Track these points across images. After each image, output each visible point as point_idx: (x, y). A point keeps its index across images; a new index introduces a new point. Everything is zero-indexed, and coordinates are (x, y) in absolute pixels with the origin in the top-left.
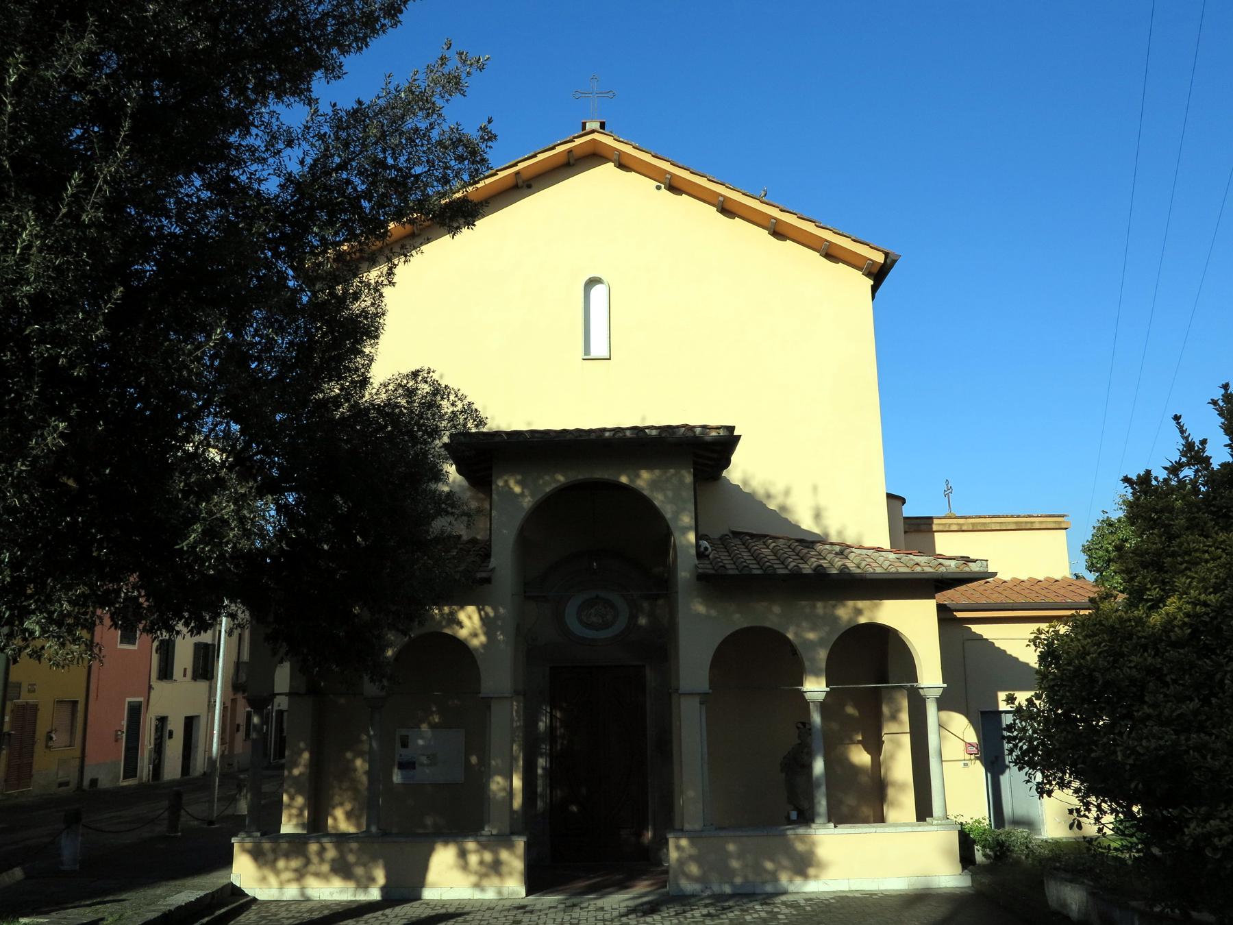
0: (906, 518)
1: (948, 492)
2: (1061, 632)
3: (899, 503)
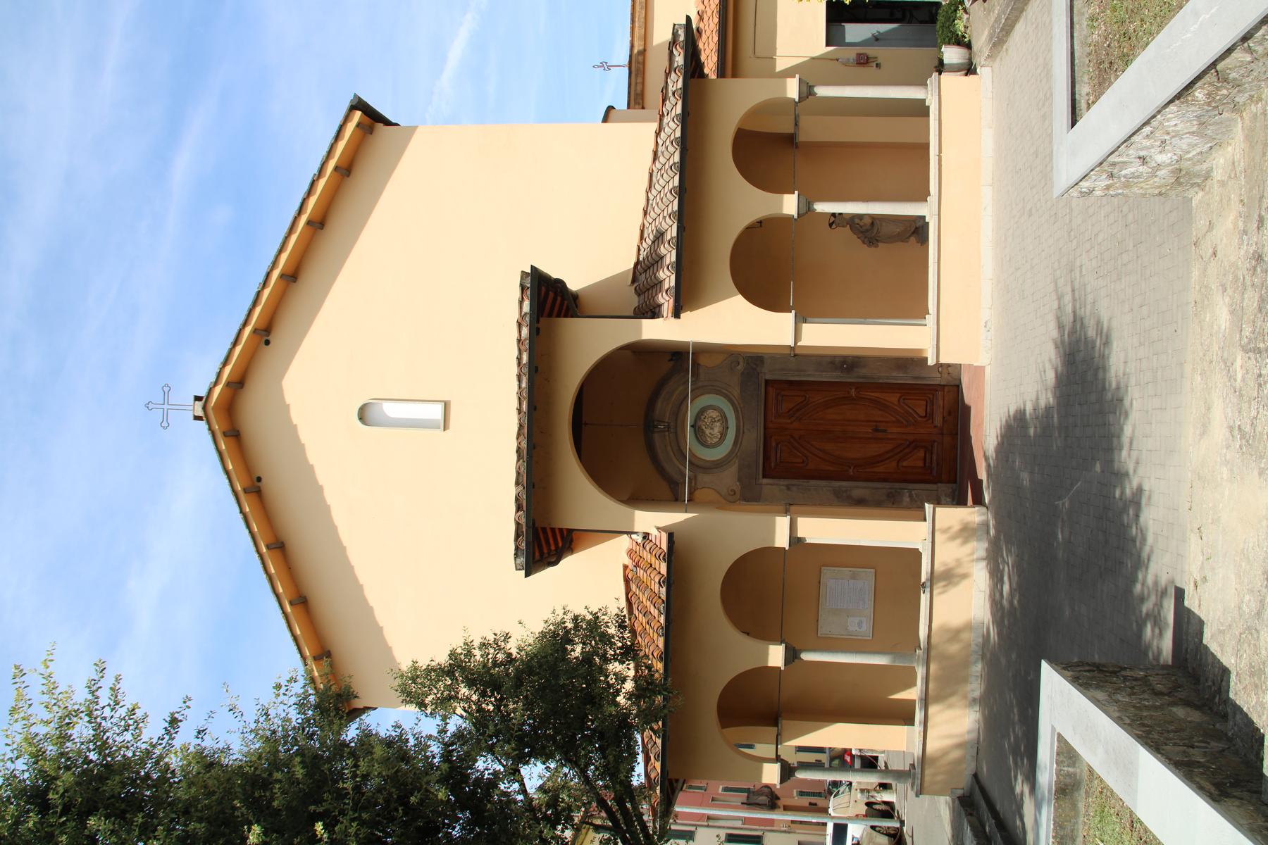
0: (629, 107)
1: (605, 66)
2: (618, 699)
3: (612, 112)
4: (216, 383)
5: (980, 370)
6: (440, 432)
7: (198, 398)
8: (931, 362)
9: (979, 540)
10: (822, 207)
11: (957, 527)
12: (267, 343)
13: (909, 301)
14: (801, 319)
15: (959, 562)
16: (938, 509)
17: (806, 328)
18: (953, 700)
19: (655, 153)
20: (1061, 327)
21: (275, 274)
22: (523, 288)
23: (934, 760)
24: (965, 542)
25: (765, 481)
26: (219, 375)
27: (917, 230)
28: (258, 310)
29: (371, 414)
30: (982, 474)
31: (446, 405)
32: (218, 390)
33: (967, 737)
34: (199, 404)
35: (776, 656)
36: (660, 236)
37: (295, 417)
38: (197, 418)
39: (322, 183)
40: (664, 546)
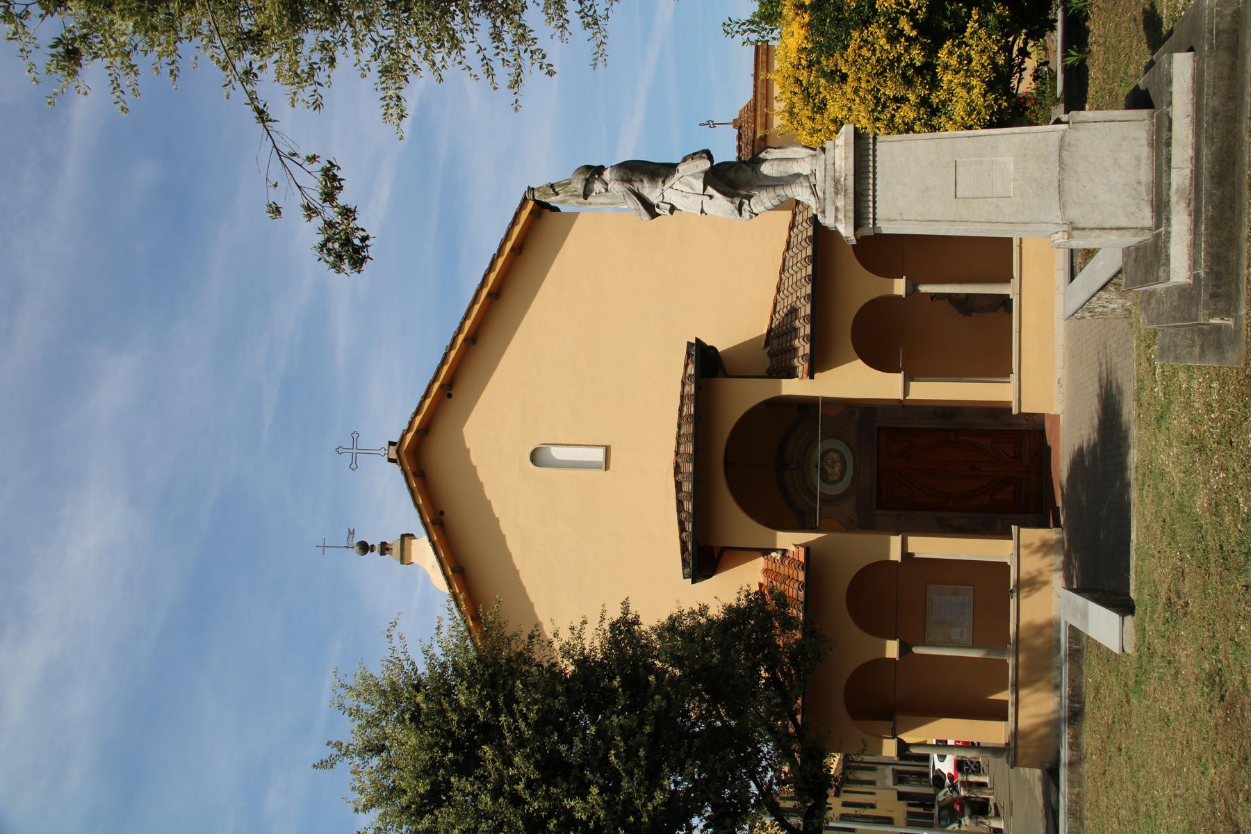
4: (408, 431)
5: (1056, 417)
6: (601, 472)
7: (391, 444)
8: (1015, 411)
9: (1056, 553)
10: (924, 289)
11: (1037, 543)
12: (450, 396)
13: (996, 360)
14: (908, 379)
15: (1040, 572)
16: (1022, 530)
17: (914, 386)
18: (1039, 685)
19: (788, 243)
20: (1101, 387)
21: (461, 338)
22: (689, 354)
23: (1026, 735)
24: (1046, 555)
25: (878, 512)
26: (411, 423)
27: (1004, 303)
28: (446, 368)
29: (541, 456)
30: (1059, 503)
31: (607, 450)
32: (409, 436)
33: (1051, 717)
34: (393, 449)
35: (892, 649)
36: (793, 312)
37: (474, 460)
38: (391, 460)
39: (501, 261)
40: (802, 559)
